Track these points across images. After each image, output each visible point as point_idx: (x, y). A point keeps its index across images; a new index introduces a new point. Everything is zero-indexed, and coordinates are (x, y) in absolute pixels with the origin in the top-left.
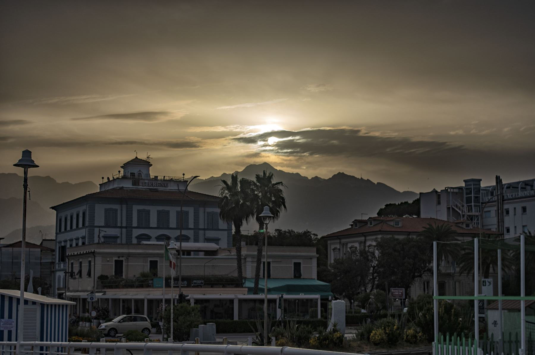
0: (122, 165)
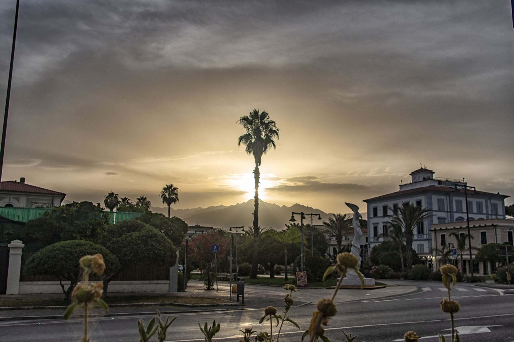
0: (411, 173)
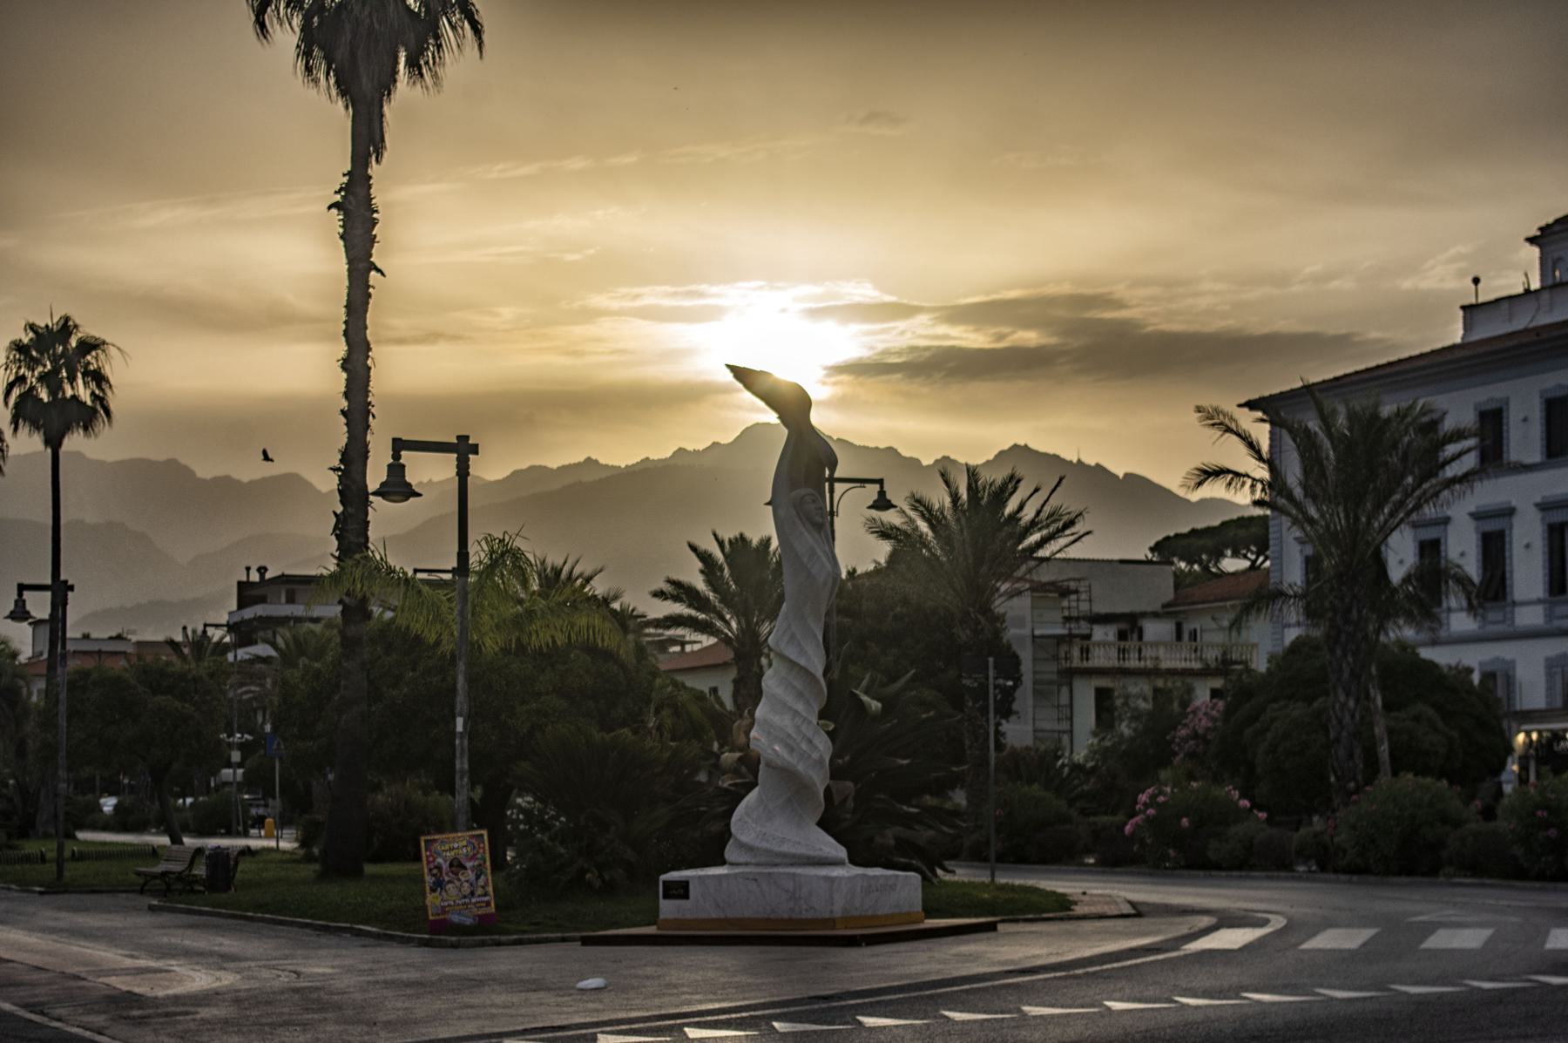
0: (1534, 232)
